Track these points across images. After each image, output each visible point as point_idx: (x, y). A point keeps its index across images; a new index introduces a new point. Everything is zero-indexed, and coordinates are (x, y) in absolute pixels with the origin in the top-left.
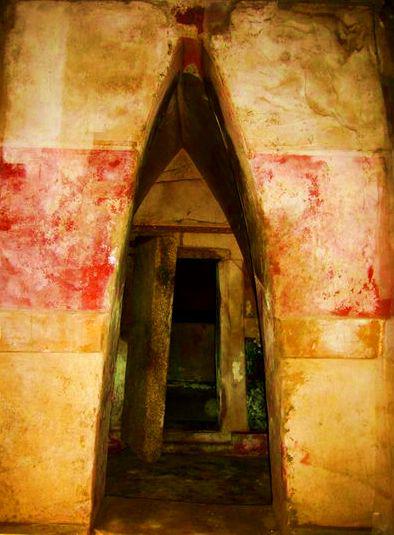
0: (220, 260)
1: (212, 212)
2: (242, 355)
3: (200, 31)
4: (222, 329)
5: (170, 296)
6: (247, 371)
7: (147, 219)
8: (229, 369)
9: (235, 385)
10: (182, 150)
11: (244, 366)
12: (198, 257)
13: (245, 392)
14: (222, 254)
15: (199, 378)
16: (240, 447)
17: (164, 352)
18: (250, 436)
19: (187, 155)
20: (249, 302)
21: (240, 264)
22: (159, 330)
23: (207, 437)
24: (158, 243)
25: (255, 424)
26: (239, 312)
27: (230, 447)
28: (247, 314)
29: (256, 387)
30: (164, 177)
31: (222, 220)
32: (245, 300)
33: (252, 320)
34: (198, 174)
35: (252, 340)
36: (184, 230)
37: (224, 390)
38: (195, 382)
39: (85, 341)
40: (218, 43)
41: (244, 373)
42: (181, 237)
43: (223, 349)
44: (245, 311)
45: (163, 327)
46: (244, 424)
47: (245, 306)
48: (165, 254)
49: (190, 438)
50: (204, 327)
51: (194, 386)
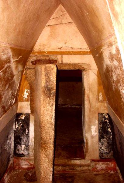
0: (84, 70)
1: (80, 43)
2: (97, 122)
3: (108, 128)
4: (86, 109)
5: (53, 104)
6: (99, 130)
7: (42, 48)
8: (90, 129)
9: (92, 137)
10: (61, 5)
11: (97, 128)
12: (72, 68)
13: (98, 141)
14: (85, 67)
15: (75, 103)
16: (95, 169)
17: (50, 139)
18: (101, 163)
19: (63, 8)
20: (100, 94)
21: (96, 72)
22: (46, 127)
23: (78, 162)
24: (43, 70)
25: (102, 156)
26: (95, 100)
27: (90, 168)
28: (100, 100)
29: (104, 138)
30: (51, 22)
31: (85, 46)
32: (99, 92)
33: (103, 104)
34: (70, 20)
35: (102, 114)
36: (62, 53)
37: (87, 140)
38: (74, 105)
39: (41, 68)
40: (81, 107)
41: (98, 131)
42: (62, 57)
43: (87, 119)
44: (98, 99)
45: (48, 125)
46: (97, 156)
47: (98, 96)
48: (49, 77)
49: (69, 163)
50: (77, 83)
51: (73, 106)
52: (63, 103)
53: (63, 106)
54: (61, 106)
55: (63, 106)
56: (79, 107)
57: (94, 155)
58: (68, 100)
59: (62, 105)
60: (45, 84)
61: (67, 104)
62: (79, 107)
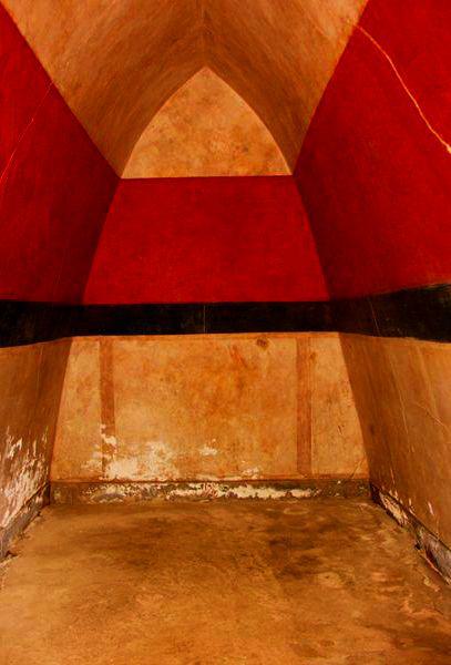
15: (253, 472)
38: (244, 483)
51: (241, 492)
52: (177, 475)
53: (179, 492)
54: (164, 490)
55: (179, 492)
56: (277, 494)
57: (153, 370)
58: (207, 451)
59: (170, 481)
60: (280, 601)
61: (200, 477)
62: (282, 493)
